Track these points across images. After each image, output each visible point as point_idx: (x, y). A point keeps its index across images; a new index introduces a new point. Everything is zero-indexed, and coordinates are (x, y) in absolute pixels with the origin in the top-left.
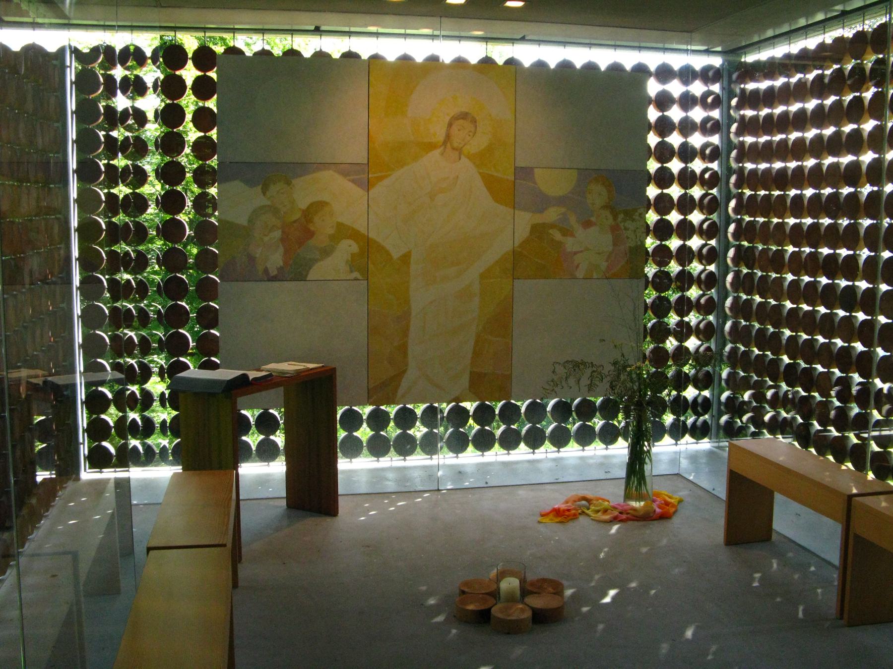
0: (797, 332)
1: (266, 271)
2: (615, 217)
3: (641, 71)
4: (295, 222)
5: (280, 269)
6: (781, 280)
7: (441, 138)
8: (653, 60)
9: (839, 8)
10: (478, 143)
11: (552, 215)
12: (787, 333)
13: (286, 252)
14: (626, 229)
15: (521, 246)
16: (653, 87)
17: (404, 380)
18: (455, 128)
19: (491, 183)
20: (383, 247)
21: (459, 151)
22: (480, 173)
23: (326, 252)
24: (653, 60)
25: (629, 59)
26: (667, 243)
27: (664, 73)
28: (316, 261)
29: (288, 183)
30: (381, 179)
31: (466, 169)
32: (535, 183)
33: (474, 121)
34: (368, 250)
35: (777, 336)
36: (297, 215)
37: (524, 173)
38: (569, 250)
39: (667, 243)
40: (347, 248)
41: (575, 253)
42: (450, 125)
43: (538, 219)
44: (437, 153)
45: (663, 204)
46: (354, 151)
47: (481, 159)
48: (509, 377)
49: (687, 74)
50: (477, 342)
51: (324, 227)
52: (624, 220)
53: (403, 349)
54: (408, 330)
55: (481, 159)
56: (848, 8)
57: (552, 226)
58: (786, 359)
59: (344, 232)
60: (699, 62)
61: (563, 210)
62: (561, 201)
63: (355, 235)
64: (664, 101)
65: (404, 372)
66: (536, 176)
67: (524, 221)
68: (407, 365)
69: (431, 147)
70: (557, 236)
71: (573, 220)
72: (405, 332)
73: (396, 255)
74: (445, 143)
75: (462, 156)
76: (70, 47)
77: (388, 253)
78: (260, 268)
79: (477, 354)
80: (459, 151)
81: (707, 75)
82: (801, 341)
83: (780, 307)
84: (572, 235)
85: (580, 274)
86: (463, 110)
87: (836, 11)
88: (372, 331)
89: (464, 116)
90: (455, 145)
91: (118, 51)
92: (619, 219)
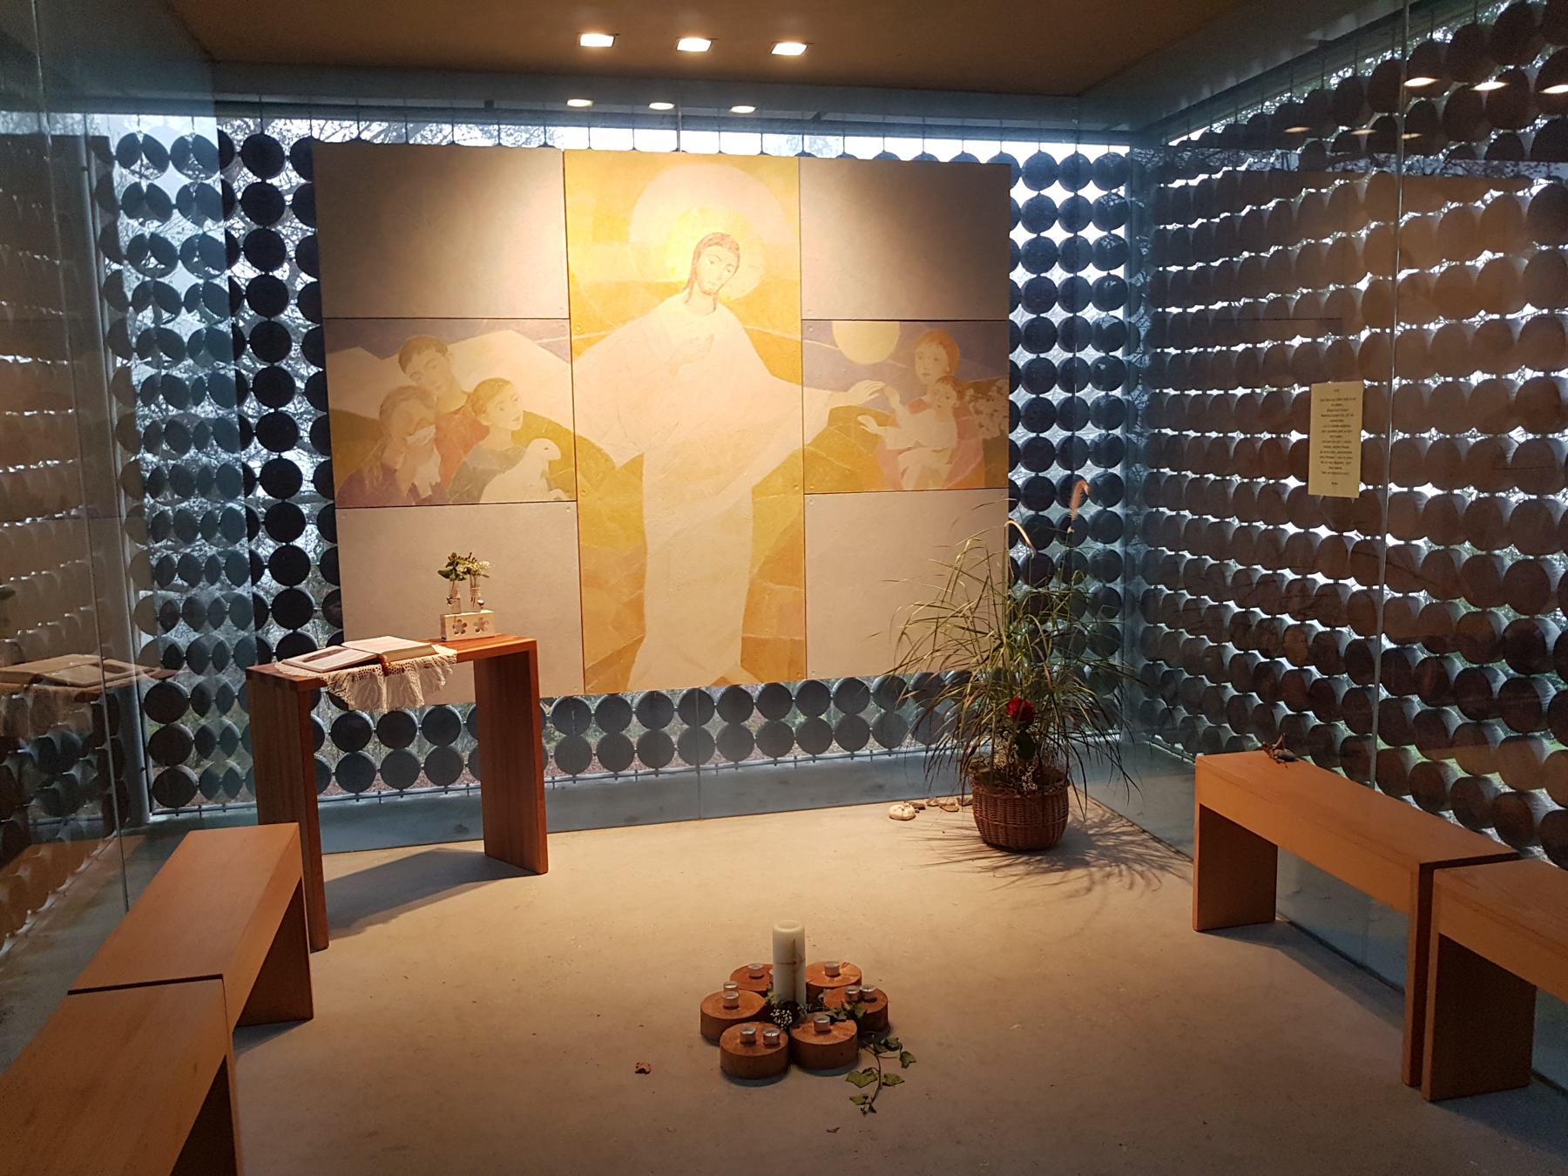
0: (1250, 522)
1: (413, 490)
2: (961, 395)
3: (1004, 170)
4: (456, 412)
5: (436, 488)
6: (1224, 484)
7: (685, 277)
8: (1022, 151)
9: (1317, 35)
10: (745, 282)
11: (862, 393)
12: (1234, 566)
13: (444, 460)
14: (978, 412)
15: (815, 443)
16: (1021, 194)
17: (639, 653)
18: (705, 260)
19: (765, 346)
20: (599, 450)
21: (713, 295)
22: (747, 331)
23: (510, 460)
24: (1022, 151)
25: (984, 150)
26: (1047, 275)
27: (1041, 172)
28: (492, 474)
29: (443, 350)
30: (589, 342)
31: (724, 325)
32: (834, 343)
33: (736, 249)
34: (575, 462)
35: (1220, 570)
36: (460, 402)
37: (816, 327)
38: (889, 448)
39: (1047, 275)
40: (543, 452)
41: (901, 452)
42: (697, 255)
43: (842, 400)
44: (678, 299)
45: (1040, 256)
46: (550, 300)
47: (746, 308)
48: (803, 645)
49: (1074, 173)
50: (751, 593)
51: (503, 421)
52: (975, 399)
53: (637, 606)
54: (643, 576)
55: (746, 308)
56: (1330, 38)
57: (863, 411)
58: (1232, 649)
59: (534, 427)
60: (1092, 152)
61: (881, 384)
62: (875, 372)
63: (553, 431)
64: (1040, 215)
65: (641, 640)
66: (835, 331)
67: (819, 405)
68: (643, 630)
69: (670, 290)
70: (872, 426)
71: (895, 401)
72: (639, 579)
73: (619, 460)
74: (690, 283)
75: (719, 305)
76: (86, 135)
77: (607, 459)
78: (404, 488)
79: (751, 611)
80: (713, 295)
81: (1106, 173)
82: (1256, 579)
83: (1219, 652)
84: (894, 424)
85: (908, 484)
86: (719, 230)
87: (1312, 42)
88: (586, 581)
89: (719, 240)
90: (707, 287)
91: (186, 339)
92: (967, 398)
